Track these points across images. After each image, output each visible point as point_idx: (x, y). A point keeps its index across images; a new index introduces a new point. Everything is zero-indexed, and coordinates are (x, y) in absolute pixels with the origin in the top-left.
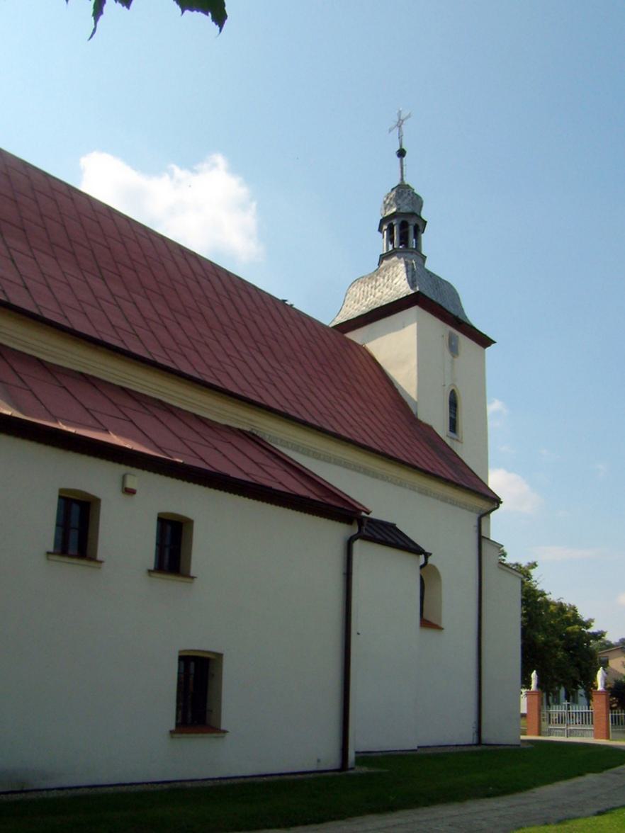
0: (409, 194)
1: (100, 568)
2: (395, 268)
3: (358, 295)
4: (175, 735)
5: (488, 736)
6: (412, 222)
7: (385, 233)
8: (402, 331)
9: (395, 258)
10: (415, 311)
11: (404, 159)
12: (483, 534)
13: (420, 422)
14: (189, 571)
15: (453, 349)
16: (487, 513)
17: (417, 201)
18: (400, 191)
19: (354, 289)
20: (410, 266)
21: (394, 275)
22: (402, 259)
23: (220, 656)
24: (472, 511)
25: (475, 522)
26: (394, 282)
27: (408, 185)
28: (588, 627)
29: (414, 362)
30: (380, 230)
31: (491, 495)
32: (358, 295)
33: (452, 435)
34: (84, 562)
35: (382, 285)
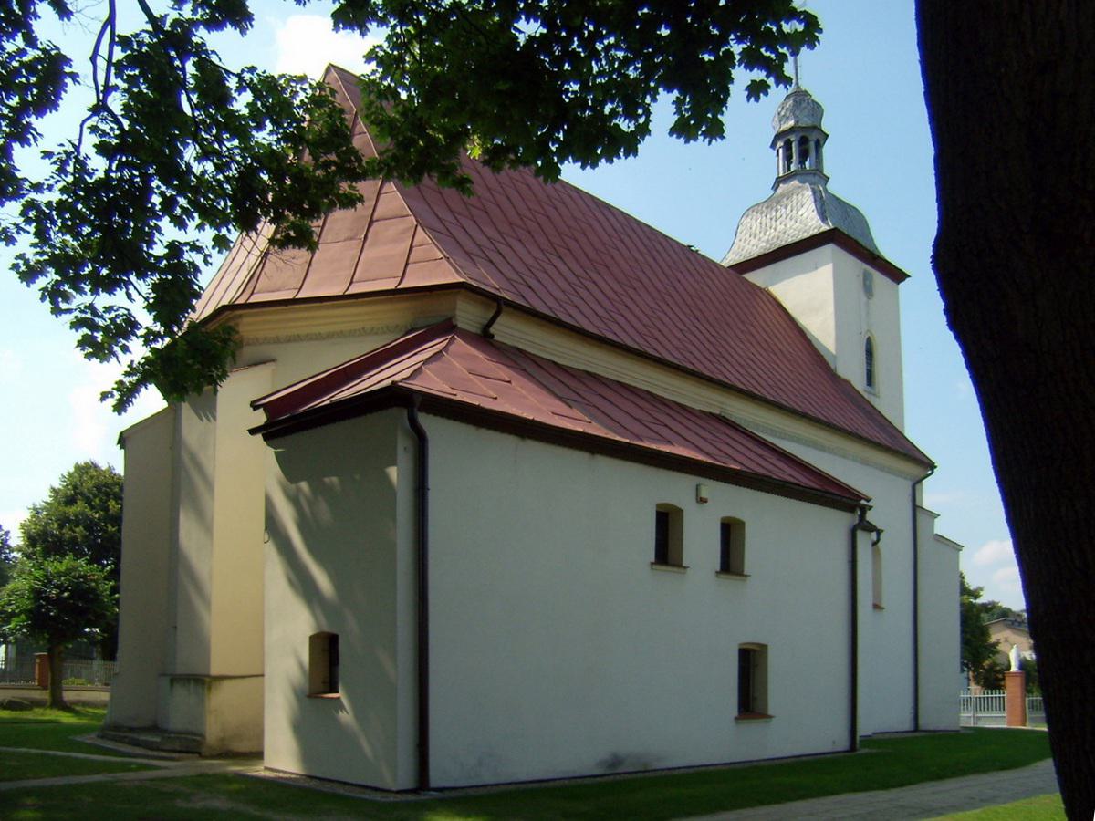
0: (808, 103)
1: (684, 573)
2: (800, 197)
3: (754, 228)
4: (740, 721)
5: (925, 723)
6: (813, 137)
7: (781, 151)
8: (814, 272)
9: (795, 183)
10: (829, 250)
11: (798, 57)
12: (918, 504)
13: (839, 377)
14: (743, 571)
15: (868, 290)
16: (919, 481)
17: (817, 110)
18: (797, 100)
19: (749, 220)
20: (818, 194)
21: (799, 204)
22: (807, 185)
23: (764, 647)
24: (906, 478)
25: (909, 490)
26: (800, 213)
27: (806, 92)
28: (977, 597)
29: (831, 309)
30: (773, 145)
31: (926, 461)
32: (754, 228)
33: (869, 389)
34: (664, 568)
35: (784, 216)
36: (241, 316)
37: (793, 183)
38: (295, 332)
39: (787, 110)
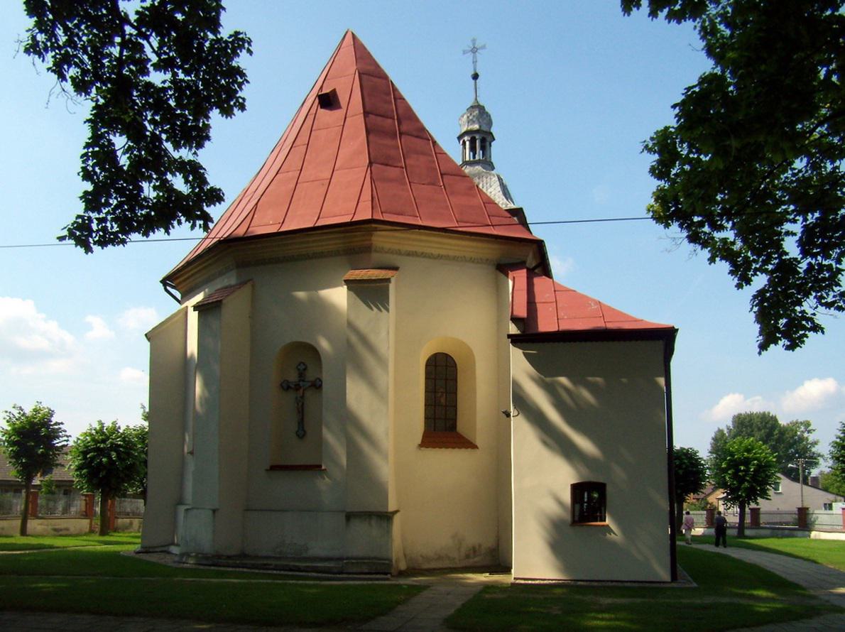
6: (489, 139)
11: (477, 81)
36: (376, 230)
37: (477, 167)
38: (414, 249)
39: (474, 116)
